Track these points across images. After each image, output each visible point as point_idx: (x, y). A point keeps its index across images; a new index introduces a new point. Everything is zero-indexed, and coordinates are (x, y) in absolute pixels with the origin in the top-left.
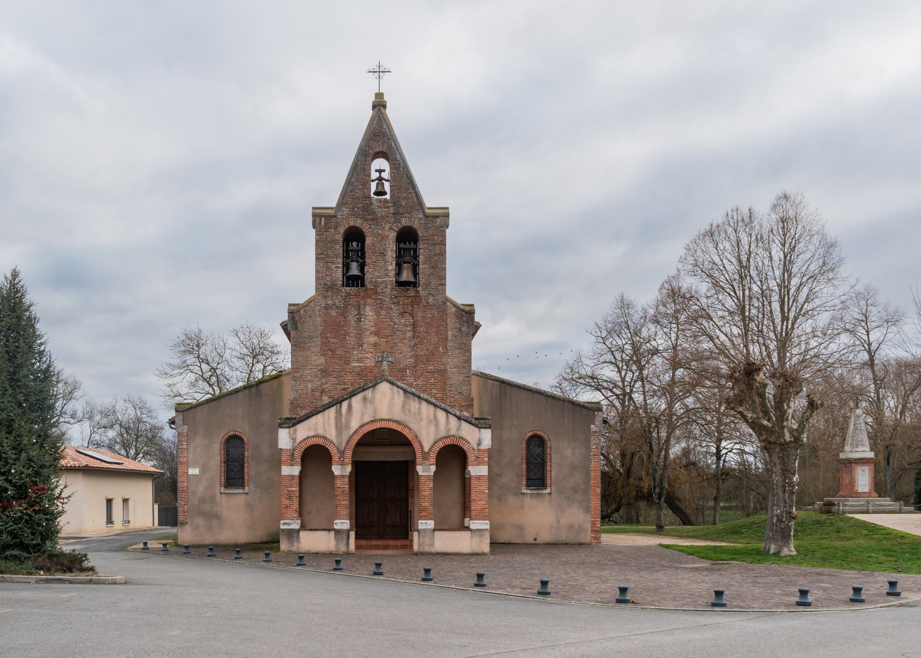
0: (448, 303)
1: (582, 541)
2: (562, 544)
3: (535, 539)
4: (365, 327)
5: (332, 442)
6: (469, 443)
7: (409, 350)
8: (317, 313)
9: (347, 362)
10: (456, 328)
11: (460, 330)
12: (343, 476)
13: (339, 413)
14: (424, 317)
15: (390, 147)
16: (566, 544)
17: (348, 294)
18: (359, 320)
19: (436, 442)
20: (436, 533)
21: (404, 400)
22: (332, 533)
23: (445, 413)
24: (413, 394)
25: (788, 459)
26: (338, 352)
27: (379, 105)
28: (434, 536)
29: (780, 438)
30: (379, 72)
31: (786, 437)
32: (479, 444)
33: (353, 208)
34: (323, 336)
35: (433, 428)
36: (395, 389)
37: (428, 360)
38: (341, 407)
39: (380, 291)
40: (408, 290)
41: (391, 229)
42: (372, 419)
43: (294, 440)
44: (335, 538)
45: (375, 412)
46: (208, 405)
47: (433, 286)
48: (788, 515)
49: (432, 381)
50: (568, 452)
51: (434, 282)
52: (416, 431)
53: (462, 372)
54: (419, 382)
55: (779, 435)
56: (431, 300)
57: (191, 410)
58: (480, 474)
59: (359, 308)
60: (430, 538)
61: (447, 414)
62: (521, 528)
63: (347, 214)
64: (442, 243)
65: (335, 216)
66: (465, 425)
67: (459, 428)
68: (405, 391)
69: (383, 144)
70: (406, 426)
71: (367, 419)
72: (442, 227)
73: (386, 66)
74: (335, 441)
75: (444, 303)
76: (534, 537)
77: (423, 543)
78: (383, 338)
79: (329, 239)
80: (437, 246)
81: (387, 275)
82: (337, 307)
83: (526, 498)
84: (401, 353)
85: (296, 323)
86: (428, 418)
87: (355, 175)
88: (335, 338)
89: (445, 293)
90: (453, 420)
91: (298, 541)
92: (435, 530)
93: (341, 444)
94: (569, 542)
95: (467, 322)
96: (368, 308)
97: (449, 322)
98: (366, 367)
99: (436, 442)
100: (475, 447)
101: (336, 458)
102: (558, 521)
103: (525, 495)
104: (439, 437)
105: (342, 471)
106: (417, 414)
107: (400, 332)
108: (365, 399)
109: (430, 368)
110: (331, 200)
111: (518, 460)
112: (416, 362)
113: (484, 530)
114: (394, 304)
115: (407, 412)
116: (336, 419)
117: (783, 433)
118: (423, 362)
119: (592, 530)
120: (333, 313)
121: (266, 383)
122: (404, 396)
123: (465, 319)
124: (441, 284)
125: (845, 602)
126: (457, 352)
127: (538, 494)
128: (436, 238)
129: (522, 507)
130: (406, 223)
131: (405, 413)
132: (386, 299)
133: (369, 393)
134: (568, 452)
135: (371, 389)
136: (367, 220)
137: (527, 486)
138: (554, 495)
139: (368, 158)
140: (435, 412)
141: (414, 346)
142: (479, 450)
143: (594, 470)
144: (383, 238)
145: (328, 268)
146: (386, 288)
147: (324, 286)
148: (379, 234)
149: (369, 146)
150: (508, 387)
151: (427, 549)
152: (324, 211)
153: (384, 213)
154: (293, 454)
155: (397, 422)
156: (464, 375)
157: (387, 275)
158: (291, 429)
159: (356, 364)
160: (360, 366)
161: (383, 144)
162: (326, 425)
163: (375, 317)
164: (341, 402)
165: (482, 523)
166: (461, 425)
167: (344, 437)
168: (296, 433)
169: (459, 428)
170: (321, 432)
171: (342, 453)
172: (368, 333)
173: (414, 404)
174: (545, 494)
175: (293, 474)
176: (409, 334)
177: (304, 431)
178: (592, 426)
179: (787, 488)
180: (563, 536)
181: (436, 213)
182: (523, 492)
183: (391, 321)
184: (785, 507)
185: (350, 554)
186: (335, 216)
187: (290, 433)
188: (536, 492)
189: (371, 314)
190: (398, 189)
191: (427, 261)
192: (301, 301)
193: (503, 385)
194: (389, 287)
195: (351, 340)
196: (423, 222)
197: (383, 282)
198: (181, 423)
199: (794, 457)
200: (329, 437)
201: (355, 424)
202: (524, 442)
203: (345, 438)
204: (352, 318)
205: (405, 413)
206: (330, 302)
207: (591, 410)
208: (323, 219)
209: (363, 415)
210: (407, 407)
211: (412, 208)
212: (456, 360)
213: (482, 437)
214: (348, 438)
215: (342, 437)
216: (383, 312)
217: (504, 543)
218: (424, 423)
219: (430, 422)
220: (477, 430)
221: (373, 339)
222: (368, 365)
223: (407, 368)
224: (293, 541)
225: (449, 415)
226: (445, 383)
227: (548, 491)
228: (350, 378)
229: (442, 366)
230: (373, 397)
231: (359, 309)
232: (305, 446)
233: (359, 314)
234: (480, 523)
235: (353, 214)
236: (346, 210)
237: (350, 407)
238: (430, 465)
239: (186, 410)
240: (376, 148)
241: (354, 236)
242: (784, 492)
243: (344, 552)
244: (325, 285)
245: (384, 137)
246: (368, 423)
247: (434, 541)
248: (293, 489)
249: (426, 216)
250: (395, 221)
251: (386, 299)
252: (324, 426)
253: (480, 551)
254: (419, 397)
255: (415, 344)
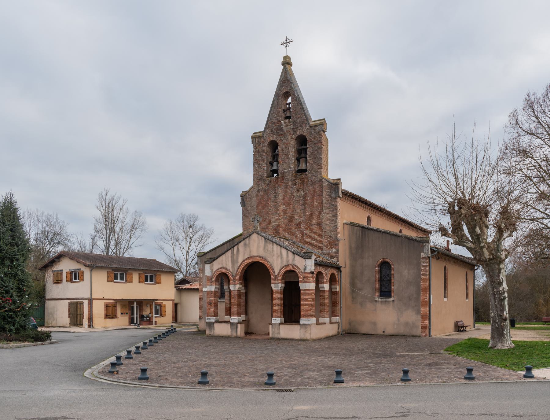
0: (323, 180)
1: (415, 334)
2: (401, 336)
3: (384, 332)
4: (278, 200)
5: (230, 271)
6: (299, 269)
7: (301, 212)
8: (255, 195)
9: (269, 223)
10: (328, 195)
11: (330, 196)
12: (235, 291)
13: (233, 253)
14: (310, 191)
15: (291, 88)
16: (404, 336)
17: (270, 182)
18: (275, 197)
19: (281, 269)
20: (281, 326)
21: (265, 243)
22: (229, 325)
23: (286, 250)
24: (269, 239)
25: (493, 273)
26: (265, 217)
27: (287, 63)
28: (280, 328)
29: (481, 256)
30: (287, 43)
31: (485, 255)
32: (305, 269)
33: (272, 130)
34: (258, 209)
35: (280, 260)
36: (260, 237)
37: (312, 217)
38: (233, 250)
39: (286, 177)
40: (301, 174)
41: (291, 138)
42: (249, 256)
43: (212, 270)
44: (231, 328)
45: (250, 252)
46: (211, 252)
47: (314, 170)
48: (499, 317)
49: (315, 230)
50: (405, 272)
51: (315, 167)
52: (271, 262)
53: (332, 223)
54: (308, 232)
55: (480, 254)
56: (313, 179)
57: (204, 256)
58: (305, 289)
59: (275, 189)
60: (278, 329)
61: (287, 251)
62: (375, 324)
63: (269, 133)
64: (319, 142)
65: (263, 136)
66: (297, 258)
67: (294, 260)
68: (265, 238)
69: (287, 87)
70: (266, 260)
71: (246, 257)
72: (320, 132)
73: (290, 38)
74: (231, 270)
75: (321, 180)
76: (383, 331)
77: (274, 332)
78: (287, 206)
79: (260, 150)
80: (317, 144)
81: (290, 167)
82: (264, 190)
83: (378, 304)
84: (297, 214)
85: (244, 202)
86: (277, 254)
87: (273, 109)
88: (263, 209)
89: (321, 174)
90: (290, 254)
91: (214, 329)
92: (280, 324)
93: (234, 272)
94: (405, 334)
95: (335, 190)
96: (279, 189)
97: (324, 192)
98: (279, 225)
99: (281, 269)
100: (303, 271)
101: (231, 281)
102: (399, 320)
103: (378, 302)
104: (283, 265)
105: (234, 288)
106: (272, 252)
107: (297, 202)
108: (245, 244)
109: (313, 222)
110: (261, 127)
111: (374, 279)
112: (306, 219)
113: (307, 324)
114: (293, 184)
115: (266, 251)
116: (231, 257)
117: (483, 252)
118: (309, 219)
119: (422, 327)
120: (262, 194)
121: (237, 238)
122: (265, 241)
123: (333, 189)
124: (319, 168)
125: (327, 384)
126: (329, 210)
127: (386, 301)
128: (316, 139)
129: (375, 310)
130: (299, 133)
131: (265, 252)
132: (289, 182)
133: (247, 241)
134: (405, 272)
135: (248, 238)
136: (279, 135)
137: (380, 296)
138: (396, 302)
139: (279, 98)
140: (281, 250)
141: (304, 209)
142: (305, 273)
143: (423, 285)
144: (287, 144)
145: (260, 168)
146: (289, 175)
147: (258, 179)
148: (285, 143)
149: (280, 90)
150: (367, 231)
151: (276, 336)
152: (257, 134)
153: (288, 130)
154: (212, 279)
155: (261, 257)
156: (333, 225)
157: (290, 167)
158: (211, 264)
159: (274, 223)
160: (276, 225)
161: (287, 87)
162: (227, 261)
163: (284, 194)
164: (233, 247)
165: (307, 320)
166: (294, 257)
167: (235, 268)
168: (213, 266)
169: (294, 260)
170: (225, 266)
171: (234, 277)
172: (280, 204)
173: (270, 246)
174: (390, 301)
175: (212, 290)
176: (302, 202)
177: (217, 265)
178: (422, 254)
179: (496, 296)
180: (402, 330)
181: (315, 124)
182: (376, 300)
183: (292, 195)
184: (497, 311)
185: (238, 337)
186: (263, 136)
187: (210, 267)
188: (384, 300)
189: (281, 192)
190: (295, 113)
191: (311, 155)
192: (247, 189)
193: (364, 229)
194: (291, 174)
195: (271, 209)
196: (309, 130)
197: (287, 172)
198: (200, 263)
199: (498, 271)
200: (228, 268)
201: (240, 260)
202: (377, 267)
203: (236, 268)
204: (271, 197)
205: (265, 252)
206: (260, 188)
207: (420, 242)
208: (257, 139)
209: (244, 254)
210: (266, 248)
211: (303, 123)
212: (328, 216)
213: (307, 265)
214: (237, 268)
215: (234, 268)
216: (288, 190)
217: (364, 334)
218: (275, 257)
219: (278, 257)
220: (303, 260)
221: (282, 207)
222: (280, 223)
223: (300, 223)
224: (211, 329)
225: (288, 251)
226: (322, 231)
227: (392, 299)
228: (271, 232)
229: (320, 220)
230: (249, 243)
231: (275, 190)
232: (217, 274)
233: (275, 193)
234: (305, 320)
235: (272, 133)
236: (268, 131)
237: (238, 249)
238: (278, 283)
239: (201, 256)
240: (284, 90)
241: (274, 146)
242: (495, 299)
243: (235, 336)
244: (258, 178)
245: (288, 82)
246: (246, 259)
247: (280, 331)
248: (212, 299)
249: (311, 127)
250: (294, 133)
251: (289, 182)
252: (226, 262)
253: (305, 338)
254: (272, 241)
255: (305, 208)
